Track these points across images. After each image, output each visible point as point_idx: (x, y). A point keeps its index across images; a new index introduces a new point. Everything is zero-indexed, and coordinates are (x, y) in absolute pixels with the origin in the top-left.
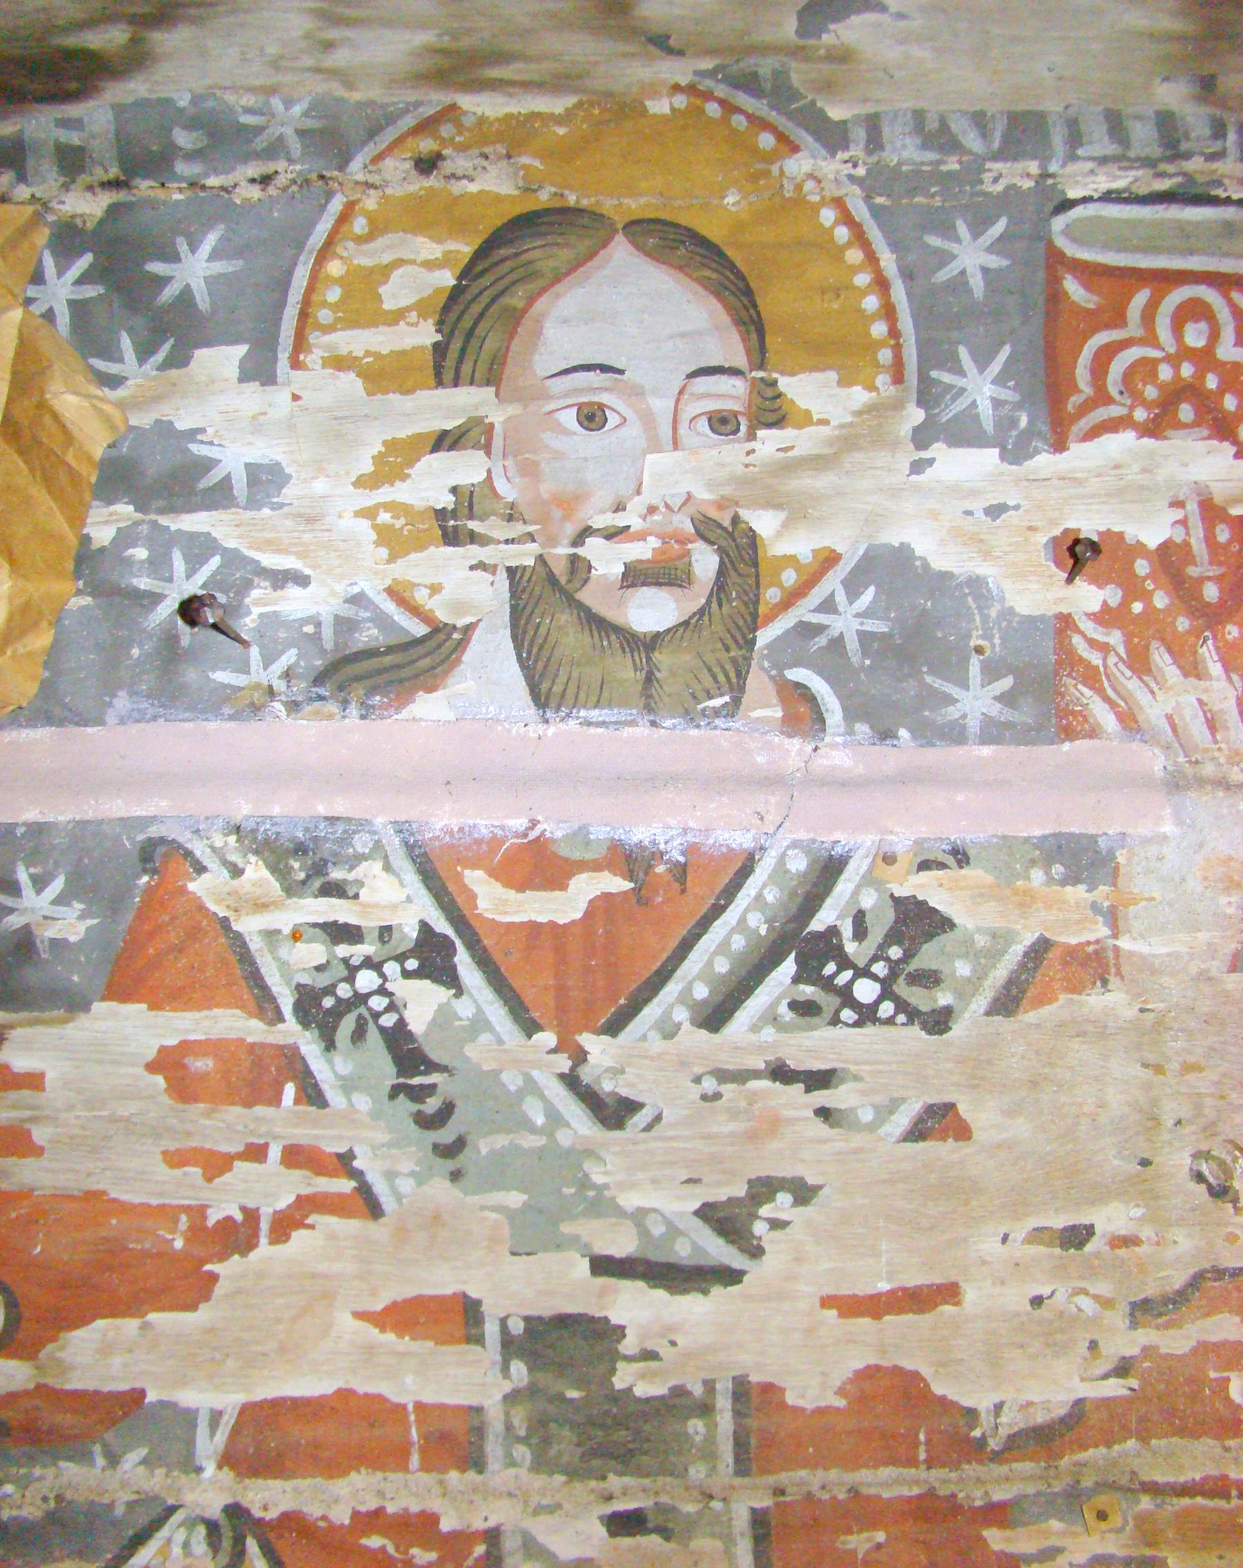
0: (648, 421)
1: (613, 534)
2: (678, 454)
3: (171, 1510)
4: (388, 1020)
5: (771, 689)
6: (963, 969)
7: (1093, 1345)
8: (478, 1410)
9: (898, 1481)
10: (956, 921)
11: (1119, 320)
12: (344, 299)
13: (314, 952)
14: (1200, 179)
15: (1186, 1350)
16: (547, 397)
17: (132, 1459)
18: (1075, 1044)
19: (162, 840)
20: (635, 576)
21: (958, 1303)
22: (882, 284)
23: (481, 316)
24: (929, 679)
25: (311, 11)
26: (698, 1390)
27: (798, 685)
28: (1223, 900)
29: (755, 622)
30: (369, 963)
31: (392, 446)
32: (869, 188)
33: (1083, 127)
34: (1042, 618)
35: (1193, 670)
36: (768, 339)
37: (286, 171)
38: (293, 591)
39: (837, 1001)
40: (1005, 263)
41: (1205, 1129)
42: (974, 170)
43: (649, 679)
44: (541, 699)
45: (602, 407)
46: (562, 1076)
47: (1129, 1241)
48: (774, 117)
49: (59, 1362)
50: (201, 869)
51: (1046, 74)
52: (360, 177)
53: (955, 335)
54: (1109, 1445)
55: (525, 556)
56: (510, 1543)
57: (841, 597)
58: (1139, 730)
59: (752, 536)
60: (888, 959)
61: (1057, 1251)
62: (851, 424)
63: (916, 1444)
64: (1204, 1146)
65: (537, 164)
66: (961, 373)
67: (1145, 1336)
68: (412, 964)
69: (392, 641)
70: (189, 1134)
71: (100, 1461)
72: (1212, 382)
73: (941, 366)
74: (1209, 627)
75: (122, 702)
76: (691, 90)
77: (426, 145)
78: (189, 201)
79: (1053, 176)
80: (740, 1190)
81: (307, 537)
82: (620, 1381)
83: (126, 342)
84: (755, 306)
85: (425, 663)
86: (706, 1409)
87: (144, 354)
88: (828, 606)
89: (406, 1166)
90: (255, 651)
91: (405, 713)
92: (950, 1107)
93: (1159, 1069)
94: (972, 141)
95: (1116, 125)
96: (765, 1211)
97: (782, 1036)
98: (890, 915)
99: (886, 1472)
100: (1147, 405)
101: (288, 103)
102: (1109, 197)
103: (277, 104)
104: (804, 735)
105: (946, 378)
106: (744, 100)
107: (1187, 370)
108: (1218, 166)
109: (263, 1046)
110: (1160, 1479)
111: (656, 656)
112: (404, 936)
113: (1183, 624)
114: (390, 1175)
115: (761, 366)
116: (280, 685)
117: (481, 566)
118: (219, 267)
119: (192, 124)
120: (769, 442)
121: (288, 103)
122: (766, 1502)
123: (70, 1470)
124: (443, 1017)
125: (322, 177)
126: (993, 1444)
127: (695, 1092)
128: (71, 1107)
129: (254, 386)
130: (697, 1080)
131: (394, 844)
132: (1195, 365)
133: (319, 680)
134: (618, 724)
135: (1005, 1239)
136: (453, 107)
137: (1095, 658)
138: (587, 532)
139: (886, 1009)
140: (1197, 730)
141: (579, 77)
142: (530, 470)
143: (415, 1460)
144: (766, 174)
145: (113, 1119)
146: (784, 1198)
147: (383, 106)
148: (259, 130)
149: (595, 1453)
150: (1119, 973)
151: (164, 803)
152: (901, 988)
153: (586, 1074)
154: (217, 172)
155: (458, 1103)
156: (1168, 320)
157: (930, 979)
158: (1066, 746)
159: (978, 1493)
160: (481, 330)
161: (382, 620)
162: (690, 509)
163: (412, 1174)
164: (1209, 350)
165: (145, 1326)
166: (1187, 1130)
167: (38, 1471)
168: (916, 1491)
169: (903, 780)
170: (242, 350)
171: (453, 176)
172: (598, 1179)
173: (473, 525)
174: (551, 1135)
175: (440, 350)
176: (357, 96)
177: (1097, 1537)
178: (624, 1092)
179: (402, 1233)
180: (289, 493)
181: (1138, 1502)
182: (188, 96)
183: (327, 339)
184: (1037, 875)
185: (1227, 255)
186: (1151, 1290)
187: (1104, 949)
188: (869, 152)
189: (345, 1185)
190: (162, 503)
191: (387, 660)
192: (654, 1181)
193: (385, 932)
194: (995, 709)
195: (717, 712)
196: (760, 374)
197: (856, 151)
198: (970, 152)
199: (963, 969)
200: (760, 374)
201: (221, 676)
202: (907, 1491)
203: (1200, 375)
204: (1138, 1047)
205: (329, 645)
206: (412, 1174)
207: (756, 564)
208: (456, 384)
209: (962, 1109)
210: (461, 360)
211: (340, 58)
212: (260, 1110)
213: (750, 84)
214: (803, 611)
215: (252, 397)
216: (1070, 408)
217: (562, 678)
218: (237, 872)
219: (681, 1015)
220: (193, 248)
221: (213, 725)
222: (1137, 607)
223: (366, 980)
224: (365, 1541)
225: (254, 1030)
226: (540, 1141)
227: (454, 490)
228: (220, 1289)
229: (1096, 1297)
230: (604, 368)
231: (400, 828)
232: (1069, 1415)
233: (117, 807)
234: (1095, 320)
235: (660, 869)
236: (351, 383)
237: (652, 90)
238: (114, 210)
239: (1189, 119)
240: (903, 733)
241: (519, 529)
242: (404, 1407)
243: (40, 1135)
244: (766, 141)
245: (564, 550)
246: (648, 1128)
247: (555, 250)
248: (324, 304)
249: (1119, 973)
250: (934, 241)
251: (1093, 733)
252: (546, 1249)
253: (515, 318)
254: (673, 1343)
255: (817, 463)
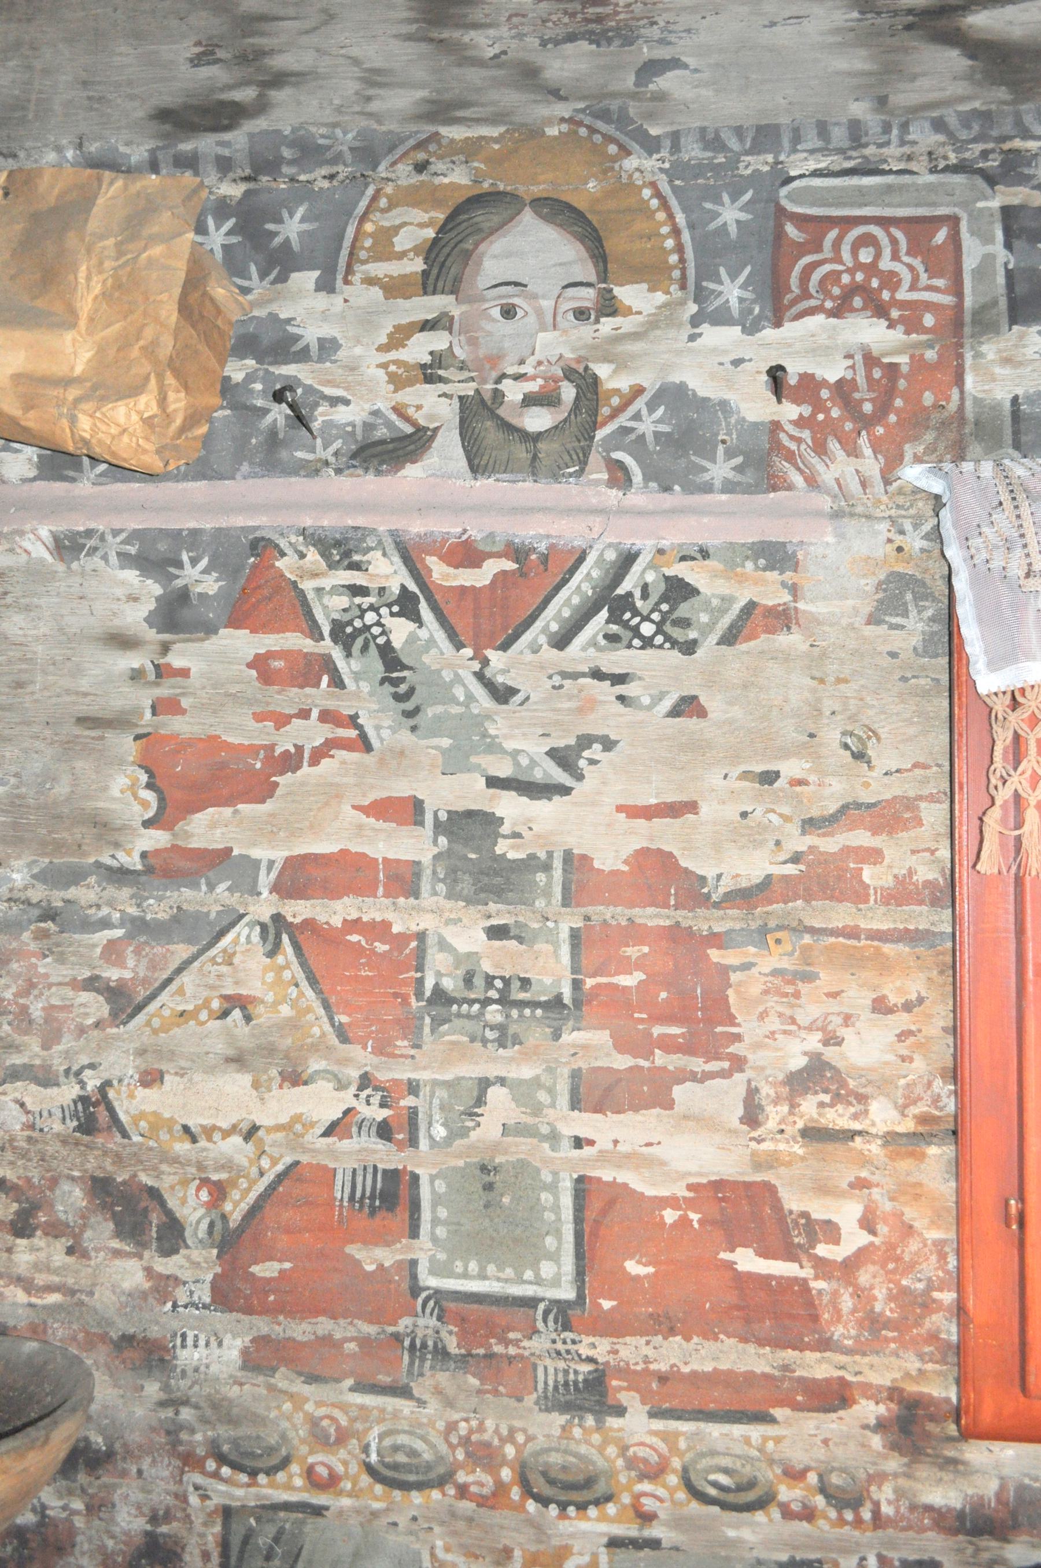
0: (539, 313)
1: (518, 377)
2: (557, 333)
3: (242, 916)
4: (381, 640)
5: (603, 464)
6: (704, 618)
7: (778, 843)
8: (418, 863)
9: (657, 916)
10: (701, 590)
11: (819, 249)
12: (374, 245)
13: (344, 601)
14: (872, 159)
15: (836, 850)
16: (484, 300)
17: (221, 888)
18: (770, 664)
19: (263, 539)
20: (530, 401)
21: (697, 813)
22: (676, 232)
23: (449, 255)
24: (693, 458)
25: (360, 79)
26: (542, 855)
27: (618, 461)
28: (863, 582)
29: (594, 426)
30: (372, 608)
31: (398, 328)
32: (671, 175)
33: (802, 133)
34: (762, 423)
35: (853, 452)
36: (609, 266)
37: (344, 171)
38: (341, 408)
39: (630, 634)
40: (750, 217)
41: (849, 718)
42: (733, 163)
43: (535, 457)
44: (475, 469)
45: (514, 306)
46: (475, 674)
47: (801, 782)
48: (618, 135)
49: (186, 832)
50: (283, 554)
51: (782, 101)
52: (383, 175)
53: (718, 260)
54: (785, 903)
55: (469, 389)
56: (431, 941)
57: (644, 412)
58: (818, 487)
59: (596, 379)
60: (660, 611)
61: (757, 785)
62: (654, 314)
63: (670, 895)
64: (849, 728)
65: (482, 166)
66: (721, 283)
67: (810, 840)
68: (396, 609)
69: (394, 435)
70: (268, 704)
71: (204, 888)
72: (875, 283)
73: (709, 279)
74: (865, 428)
75: (245, 468)
76: (570, 120)
77: (421, 156)
78: (289, 189)
79: (781, 163)
80: (572, 741)
81: (350, 378)
82: (499, 850)
83: (253, 269)
84: (602, 247)
85: (412, 447)
86: (547, 867)
87: (263, 275)
88: (637, 417)
89: (387, 723)
90: (319, 441)
91: (399, 474)
92: (694, 698)
93: (822, 681)
94: (734, 144)
95: (823, 129)
96: (586, 754)
97: (599, 654)
98: (662, 586)
99: (650, 910)
100: (833, 298)
101: (345, 133)
102: (816, 173)
103: (338, 132)
104: (619, 488)
105: (712, 286)
106: (600, 125)
107: (859, 277)
108: (885, 151)
109: (312, 654)
110: (817, 926)
111: (540, 445)
112: (392, 593)
113: (849, 426)
114: (378, 728)
115: (605, 281)
116: (332, 459)
117: (444, 395)
118: (306, 226)
119: (292, 144)
120: (607, 325)
121: (345, 133)
122: (579, 924)
123: (187, 892)
124: (412, 639)
125: (363, 175)
126: (715, 898)
127: (549, 684)
128: (204, 688)
129: (323, 294)
130: (550, 677)
131: (388, 542)
132: (865, 273)
133: (354, 456)
134: (514, 482)
135: (726, 777)
136: (437, 133)
137: (793, 446)
138: (504, 376)
139: (659, 639)
140: (854, 486)
141: (507, 115)
142: (473, 342)
143: (381, 891)
144: (612, 169)
145: (227, 695)
146: (597, 747)
147: (398, 134)
148: (328, 148)
149: (482, 890)
150: (797, 623)
151: (264, 519)
152: (668, 628)
153: (488, 673)
154: (305, 173)
155: (418, 687)
156: (849, 247)
157: (685, 623)
158: (772, 495)
159: (706, 927)
160: (448, 264)
161: (389, 424)
162: (562, 363)
163: (389, 727)
164: (874, 264)
165: (236, 812)
166: (839, 717)
167: (168, 894)
168: (668, 923)
169: (673, 511)
170: (317, 273)
171: (436, 174)
172: (492, 732)
173: (440, 372)
174: (467, 707)
175: (425, 274)
176: (384, 128)
177: (777, 958)
178: (510, 683)
179: (382, 762)
180: (341, 354)
181: (802, 938)
182: (289, 128)
183: (364, 267)
184: (749, 565)
185: (889, 205)
186: (815, 812)
187: (788, 609)
188: (672, 154)
189: (353, 733)
190: (271, 359)
191: (391, 446)
192: (524, 734)
193: (382, 590)
194: (731, 475)
195: (571, 475)
196: (603, 285)
197: (664, 153)
198: (731, 150)
199: (704, 618)
200: (603, 285)
201: (299, 454)
202: (662, 923)
203: (868, 279)
204: (809, 668)
205: (359, 438)
206: (389, 727)
207: (597, 394)
208: (434, 293)
209: (702, 700)
210: (437, 279)
211: (374, 106)
212: (308, 690)
213: (604, 115)
214: (623, 420)
215: (321, 301)
216: (785, 302)
217: (485, 458)
218: (302, 556)
219: (543, 639)
220: (291, 215)
221: (293, 479)
222: (821, 417)
223: (370, 617)
224: (348, 937)
225: (307, 645)
226: (463, 709)
227: (431, 353)
228: (279, 792)
229: (781, 815)
230: (516, 284)
231: (393, 534)
232: (762, 883)
233: (239, 521)
234: (803, 249)
235: (533, 557)
236: (377, 293)
237: (549, 122)
238: (247, 193)
239: (870, 123)
240: (677, 488)
241: (466, 374)
242: (377, 860)
243: (185, 703)
244: (613, 149)
245: (490, 386)
246: (521, 704)
247: (492, 216)
248: (363, 248)
249: (797, 623)
250: (708, 205)
251: (790, 487)
252: (462, 772)
253: (467, 255)
254: (530, 829)
255: (635, 336)
